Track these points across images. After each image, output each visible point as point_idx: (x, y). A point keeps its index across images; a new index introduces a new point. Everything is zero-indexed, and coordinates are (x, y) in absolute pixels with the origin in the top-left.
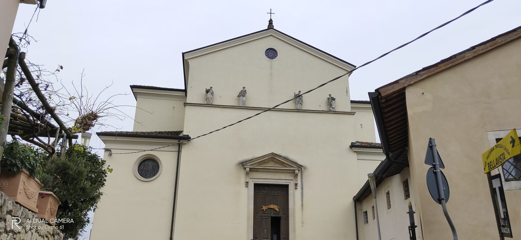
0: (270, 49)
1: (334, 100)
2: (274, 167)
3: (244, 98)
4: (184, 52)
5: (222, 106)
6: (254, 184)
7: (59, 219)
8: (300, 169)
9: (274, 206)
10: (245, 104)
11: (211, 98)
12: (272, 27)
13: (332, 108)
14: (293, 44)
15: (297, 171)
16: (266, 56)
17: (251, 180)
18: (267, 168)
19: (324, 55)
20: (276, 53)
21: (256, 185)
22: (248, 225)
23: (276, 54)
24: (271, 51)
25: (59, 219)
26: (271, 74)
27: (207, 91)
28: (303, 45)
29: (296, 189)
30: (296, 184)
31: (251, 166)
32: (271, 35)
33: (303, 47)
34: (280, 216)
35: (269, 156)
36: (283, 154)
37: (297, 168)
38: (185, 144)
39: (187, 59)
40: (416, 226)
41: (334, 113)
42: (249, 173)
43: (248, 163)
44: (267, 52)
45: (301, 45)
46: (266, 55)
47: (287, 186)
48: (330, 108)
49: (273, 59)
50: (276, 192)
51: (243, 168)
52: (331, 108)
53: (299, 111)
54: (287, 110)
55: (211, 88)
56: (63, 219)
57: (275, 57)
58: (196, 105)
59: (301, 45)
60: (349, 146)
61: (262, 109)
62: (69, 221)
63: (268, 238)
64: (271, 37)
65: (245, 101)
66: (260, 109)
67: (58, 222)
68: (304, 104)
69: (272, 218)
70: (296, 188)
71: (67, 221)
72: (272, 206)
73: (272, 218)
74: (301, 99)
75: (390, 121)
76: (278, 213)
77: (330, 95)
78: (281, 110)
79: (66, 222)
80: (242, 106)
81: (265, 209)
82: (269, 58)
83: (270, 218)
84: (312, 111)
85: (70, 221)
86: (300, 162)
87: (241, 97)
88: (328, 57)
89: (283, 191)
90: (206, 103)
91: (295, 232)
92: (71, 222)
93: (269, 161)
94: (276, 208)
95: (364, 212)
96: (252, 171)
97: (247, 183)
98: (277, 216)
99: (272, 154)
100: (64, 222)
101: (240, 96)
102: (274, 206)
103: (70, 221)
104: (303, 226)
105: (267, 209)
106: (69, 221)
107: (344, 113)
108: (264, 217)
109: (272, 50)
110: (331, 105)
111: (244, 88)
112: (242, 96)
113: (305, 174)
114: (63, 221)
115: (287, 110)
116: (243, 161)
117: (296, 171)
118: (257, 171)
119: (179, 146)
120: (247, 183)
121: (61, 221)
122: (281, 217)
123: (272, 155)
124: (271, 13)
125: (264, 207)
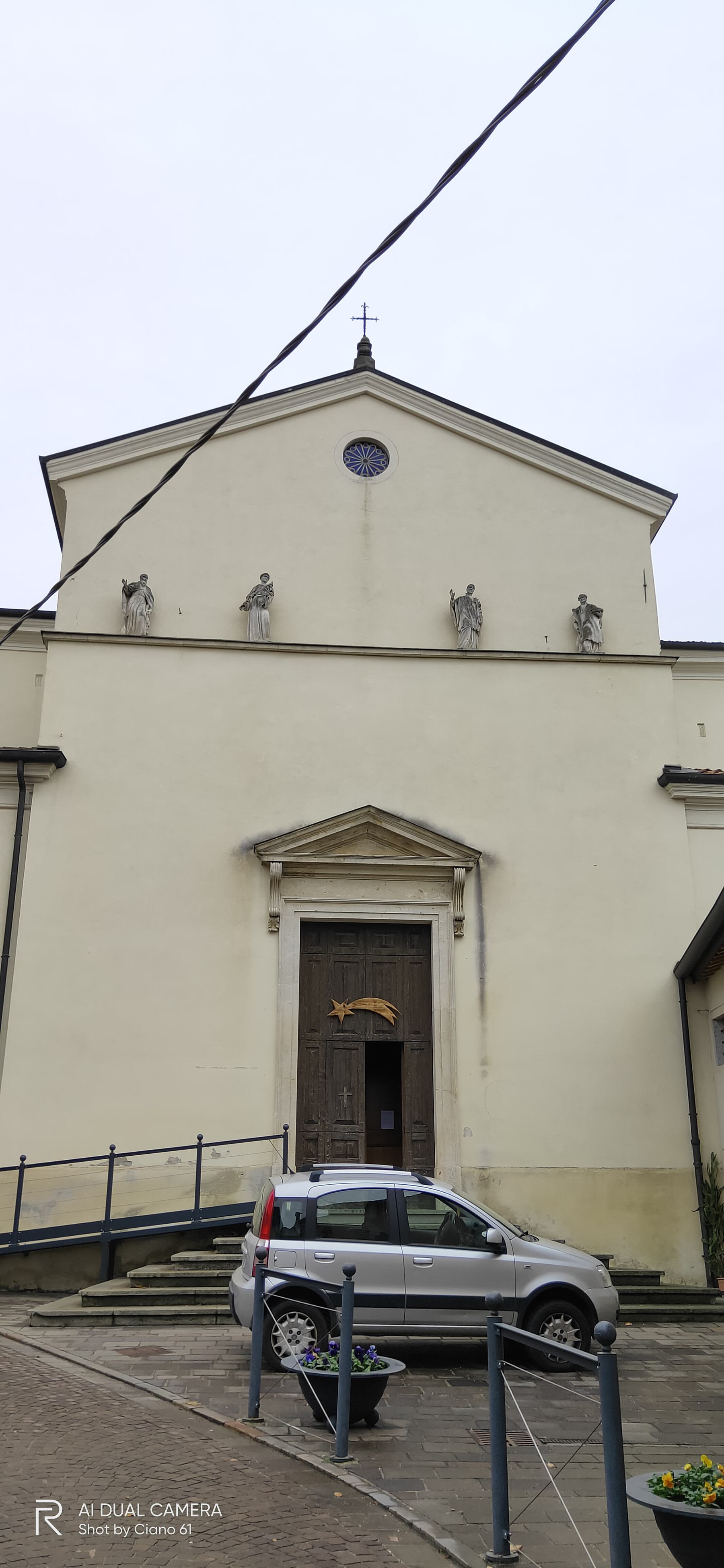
0: (362, 443)
1: (598, 617)
2: (373, 857)
3: (265, 613)
4: (45, 454)
5: (181, 643)
6: (301, 922)
7: (178, 1505)
8: (471, 864)
9: (375, 1002)
10: (268, 636)
11: (141, 614)
12: (368, 364)
13: (590, 644)
15: (460, 873)
16: (348, 466)
17: (291, 908)
18: (347, 861)
19: (558, 458)
20: (382, 457)
21: (309, 928)
22: (279, 1073)
23: (383, 460)
24: (366, 450)
25: (178, 1505)
26: (366, 530)
27: (129, 591)
28: (480, 425)
29: (458, 937)
30: (459, 921)
31: (289, 856)
32: (366, 394)
33: (482, 430)
34: (400, 1039)
35: (357, 818)
36: (410, 812)
37: (463, 861)
38: (46, 779)
39: (60, 481)
41: (599, 662)
42: (279, 881)
43: (277, 846)
44: (349, 454)
45: (476, 423)
46: (348, 462)
47: (423, 930)
48: (582, 643)
49: (371, 475)
50: (385, 951)
51: (259, 863)
52: (587, 644)
53: (469, 655)
54: (422, 653)
55: (144, 577)
57: (379, 470)
58: (85, 638)
59: (476, 423)
60: (656, 780)
61: (330, 650)
62: (206, 1511)
63: (355, 1119)
64: (365, 402)
65: (267, 624)
66: (323, 649)
67: (175, 1513)
68: (485, 632)
69: (372, 1048)
70: (459, 933)
71: (202, 1510)
72: (369, 1003)
73: (372, 1048)
74: (474, 614)
76: (392, 1027)
77: (582, 598)
78: (402, 653)
79: (199, 1513)
80: (256, 640)
81: (341, 1015)
82: (359, 473)
83: (362, 1049)
84: (516, 656)
85: (210, 1512)
86: (471, 840)
87: (254, 608)
88: (574, 465)
89: (413, 947)
90: (123, 632)
91: (456, 1096)
92: (214, 1512)
93: (356, 839)
94: (384, 1010)
95: (714, 1020)
96: (295, 874)
97: (275, 917)
98: (389, 1037)
99: (366, 810)
100: (192, 1515)
101: (251, 607)
102: (375, 1002)
103: (210, 1512)
104: (484, 1074)
105: (352, 1013)
106: (206, 1511)
107: (636, 659)
108: (341, 1045)
109: (369, 447)
110: (584, 633)
111: (265, 576)
112: (257, 603)
113: (494, 882)
115: (422, 653)
116: (262, 840)
117: (457, 871)
118: (311, 875)
119: (22, 788)
120: (275, 917)
121: (182, 1511)
122: (402, 1043)
123: (368, 814)
124: (365, 319)
125: (338, 1006)
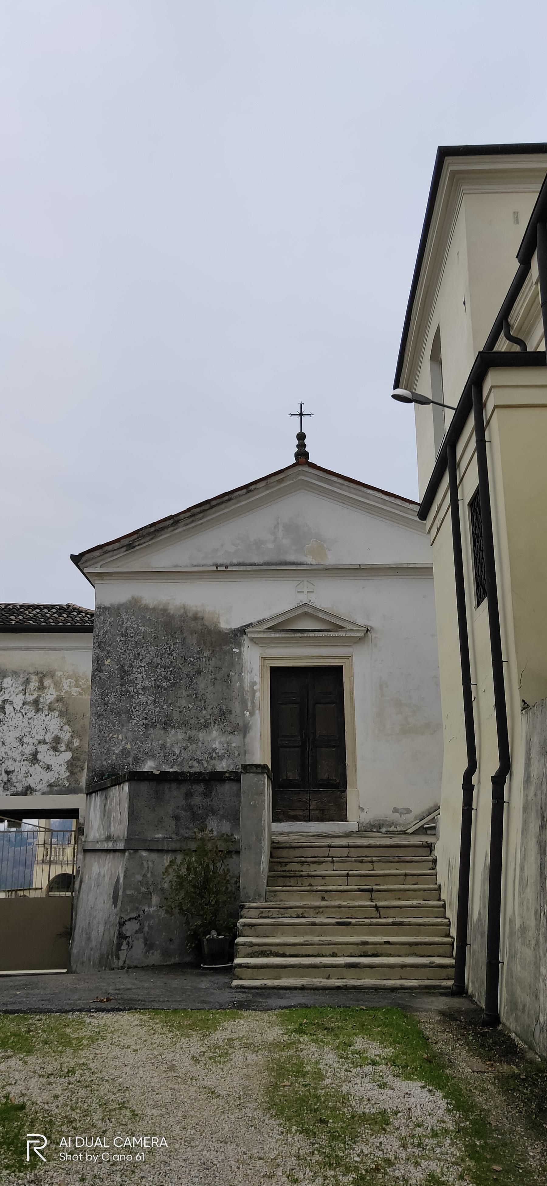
7: (134, 1138)
14: (512, 190)
40: (376, 904)
56: (143, 1139)
71: (153, 1143)
75: (413, 948)
79: (149, 1144)
92: (161, 1144)
100: (28, 1142)
114: (143, 1142)
